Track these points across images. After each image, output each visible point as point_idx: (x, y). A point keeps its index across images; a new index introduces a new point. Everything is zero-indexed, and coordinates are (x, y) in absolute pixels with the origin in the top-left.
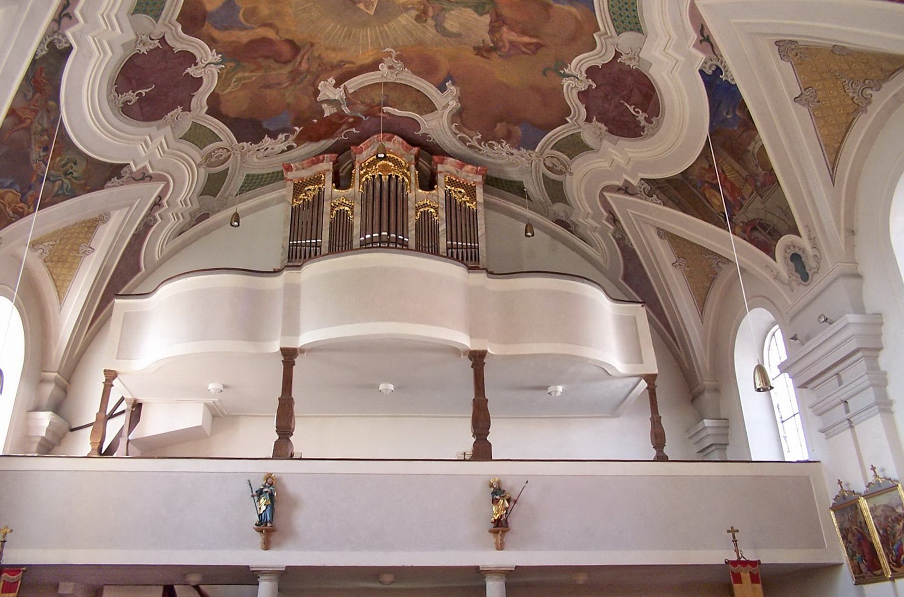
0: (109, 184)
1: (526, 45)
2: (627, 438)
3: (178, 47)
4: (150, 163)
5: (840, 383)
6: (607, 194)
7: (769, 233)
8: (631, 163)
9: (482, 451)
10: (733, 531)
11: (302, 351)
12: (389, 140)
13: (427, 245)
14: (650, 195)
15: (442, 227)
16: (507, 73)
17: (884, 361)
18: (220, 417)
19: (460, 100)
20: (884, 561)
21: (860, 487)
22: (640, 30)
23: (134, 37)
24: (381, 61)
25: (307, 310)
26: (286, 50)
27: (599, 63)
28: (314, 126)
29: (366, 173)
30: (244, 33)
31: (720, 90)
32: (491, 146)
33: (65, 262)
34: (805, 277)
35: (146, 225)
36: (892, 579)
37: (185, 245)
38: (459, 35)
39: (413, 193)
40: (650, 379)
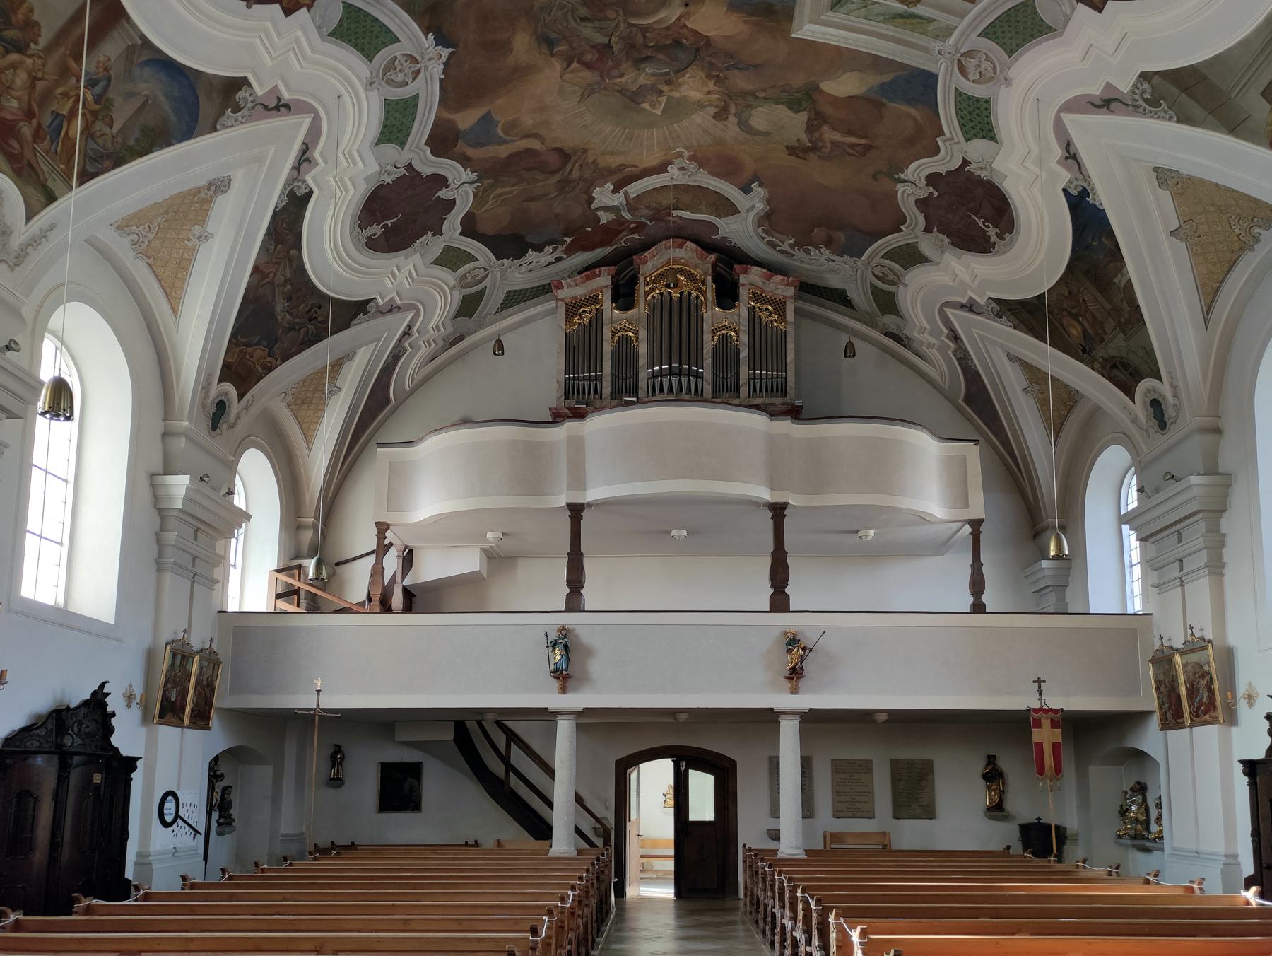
0: (355, 322)
1: (852, 146)
2: (946, 585)
3: (427, 171)
4: (282, 78)
5: (1180, 541)
6: (949, 312)
7: (1130, 374)
8: (978, 279)
9: (780, 603)
10: (1039, 682)
11: (590, 505)
12: (680, 246)
13: (724, 391)
14: (999, 315)
15: (744, 354)
16: (827, 176)
17: (1225, 524)
18: (499, 560)
19: (769, 202)
20: (1186, 710)
21: (1178, 643)
22: (993, 139)
23: (378, 168)
24: (670, 163)
25: (593, 463)
26: (554, 159)
27: (943, 170)
28: (583, 234)
29: (653, 289)
30: (503, 147)
31: (1086, 217)
32: (807, 252)
33: (310, 403)
34: (1163, 426)
35: (395, 357)
36: (1191, 727)
37: (437, 371)
38: (768, 133)
39: (709, 312)
40: (976, 525)
